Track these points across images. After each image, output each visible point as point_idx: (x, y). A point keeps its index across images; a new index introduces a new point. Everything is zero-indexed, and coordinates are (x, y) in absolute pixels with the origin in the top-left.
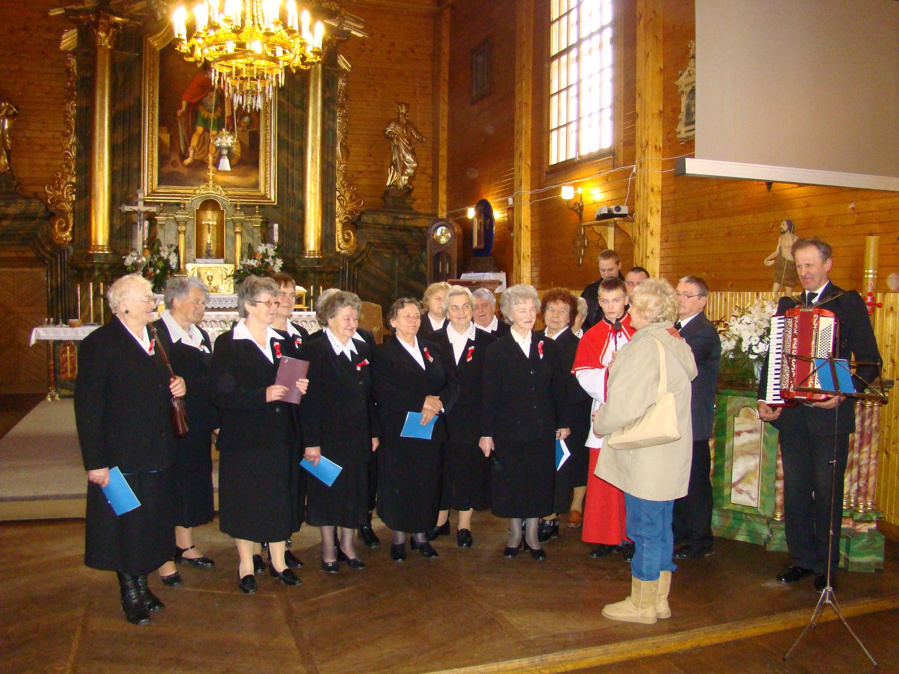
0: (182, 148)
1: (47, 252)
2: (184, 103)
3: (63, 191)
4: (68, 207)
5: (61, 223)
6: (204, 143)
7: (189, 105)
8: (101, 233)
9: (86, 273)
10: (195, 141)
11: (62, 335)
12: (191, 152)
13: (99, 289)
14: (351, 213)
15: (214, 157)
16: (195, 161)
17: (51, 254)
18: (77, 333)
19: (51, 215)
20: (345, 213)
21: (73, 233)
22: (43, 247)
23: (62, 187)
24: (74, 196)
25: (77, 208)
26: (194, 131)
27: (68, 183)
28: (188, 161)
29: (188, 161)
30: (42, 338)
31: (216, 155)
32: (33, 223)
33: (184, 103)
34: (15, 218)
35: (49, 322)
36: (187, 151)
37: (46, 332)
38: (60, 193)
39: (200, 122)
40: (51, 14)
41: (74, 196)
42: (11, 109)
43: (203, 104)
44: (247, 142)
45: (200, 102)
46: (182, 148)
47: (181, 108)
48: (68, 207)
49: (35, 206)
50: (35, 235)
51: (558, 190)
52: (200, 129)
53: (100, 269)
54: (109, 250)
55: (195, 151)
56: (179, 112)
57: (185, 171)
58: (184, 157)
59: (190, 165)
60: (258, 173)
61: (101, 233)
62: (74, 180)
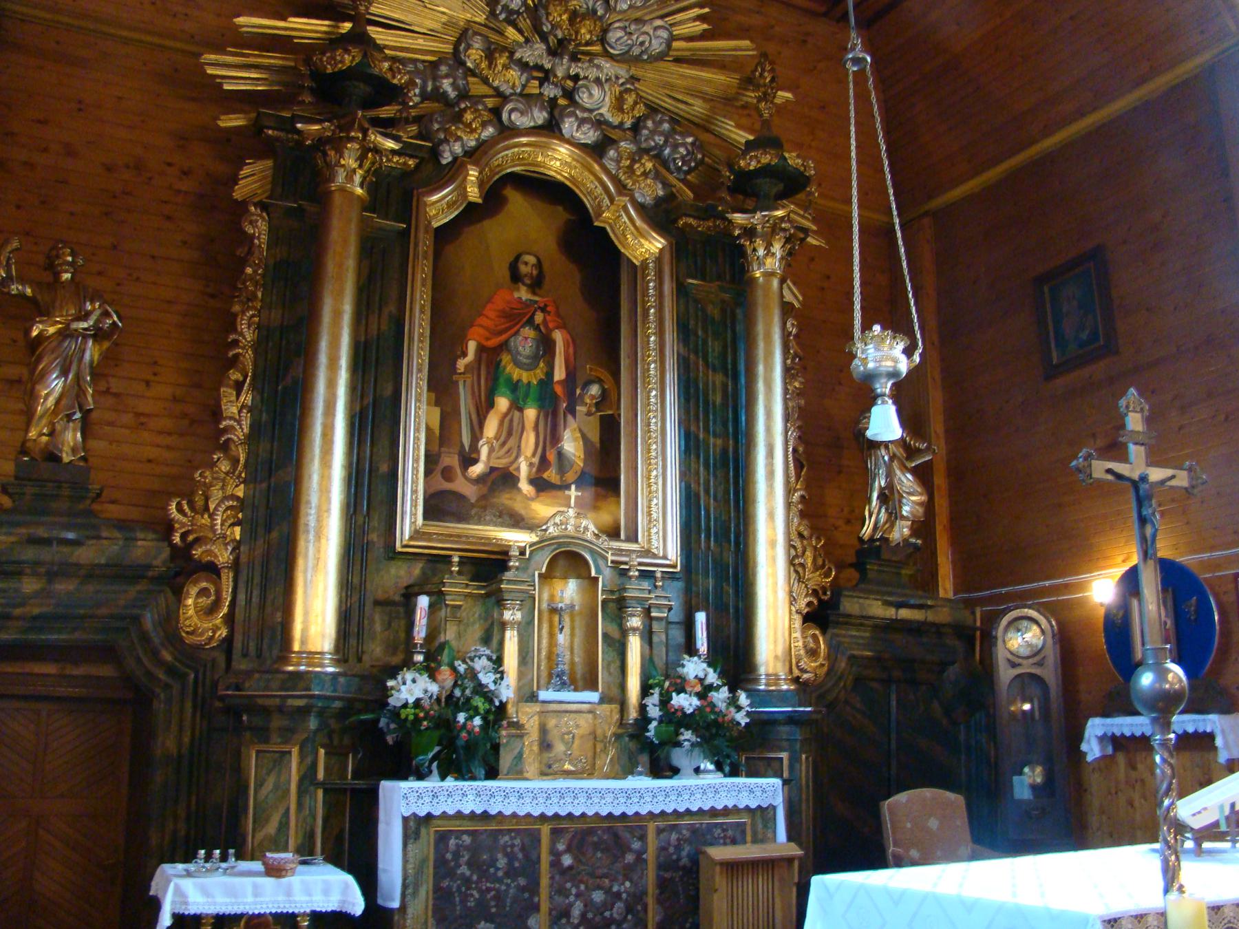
0: (466, 440)
1: (161, 663)
2: (472, 346)
3: (211, 516)
4: (223, 556)
5: (203, 592)
6: (510, 434)
7: (481, 349)
8: (316, 616)
9: (277, 722)
10: (491, 427)
11: (250, 899)
12: (484, 451)
13: (314, 765)
14: (815, 592)
15: (531, 465)
16: (493, 469)
17: (171, 670)
18: (289, 893)
19: (186, 566)
20: (807, 595)
21: (230, 619)
22: (155, 654)
23: (212, 507)
24: (238, 529)
25: (244, 559)
26: (491, 405)
27: (226, 498)
28: (477, 470)
29: (477, 470)
30: (192, 910)
31: (536, 460)
32: (133, 591)
33: (472, 346)
34: (92, 573)
35: (208, 858)
36: (475, 448)
37: (205, 892)
38: (205, 520)
39: (503, 389)
40: (222, 124)
41: (238, 529)
42: (106, 314)
43: (509, 351)
44: (595, 437)
45: (504, 347)
46: (466, 440)
47: (465, 354)
48: (223, 556)
49: (146, 548)
50: (136, 619)
51: (1082, 586)
52: (502, 403)
53: (321, 713)
54: (337, 662)
55: (491, 450)
56: (461, 364)
57: (470, 492)
58: (469, 460)
59: (480, 480)
60: (619, 503)
61: (316, 616)
62: (240, 492)
